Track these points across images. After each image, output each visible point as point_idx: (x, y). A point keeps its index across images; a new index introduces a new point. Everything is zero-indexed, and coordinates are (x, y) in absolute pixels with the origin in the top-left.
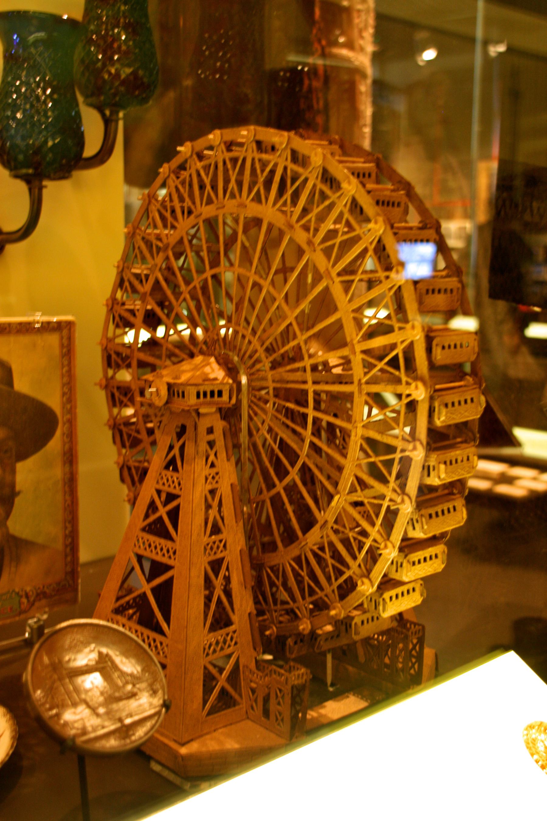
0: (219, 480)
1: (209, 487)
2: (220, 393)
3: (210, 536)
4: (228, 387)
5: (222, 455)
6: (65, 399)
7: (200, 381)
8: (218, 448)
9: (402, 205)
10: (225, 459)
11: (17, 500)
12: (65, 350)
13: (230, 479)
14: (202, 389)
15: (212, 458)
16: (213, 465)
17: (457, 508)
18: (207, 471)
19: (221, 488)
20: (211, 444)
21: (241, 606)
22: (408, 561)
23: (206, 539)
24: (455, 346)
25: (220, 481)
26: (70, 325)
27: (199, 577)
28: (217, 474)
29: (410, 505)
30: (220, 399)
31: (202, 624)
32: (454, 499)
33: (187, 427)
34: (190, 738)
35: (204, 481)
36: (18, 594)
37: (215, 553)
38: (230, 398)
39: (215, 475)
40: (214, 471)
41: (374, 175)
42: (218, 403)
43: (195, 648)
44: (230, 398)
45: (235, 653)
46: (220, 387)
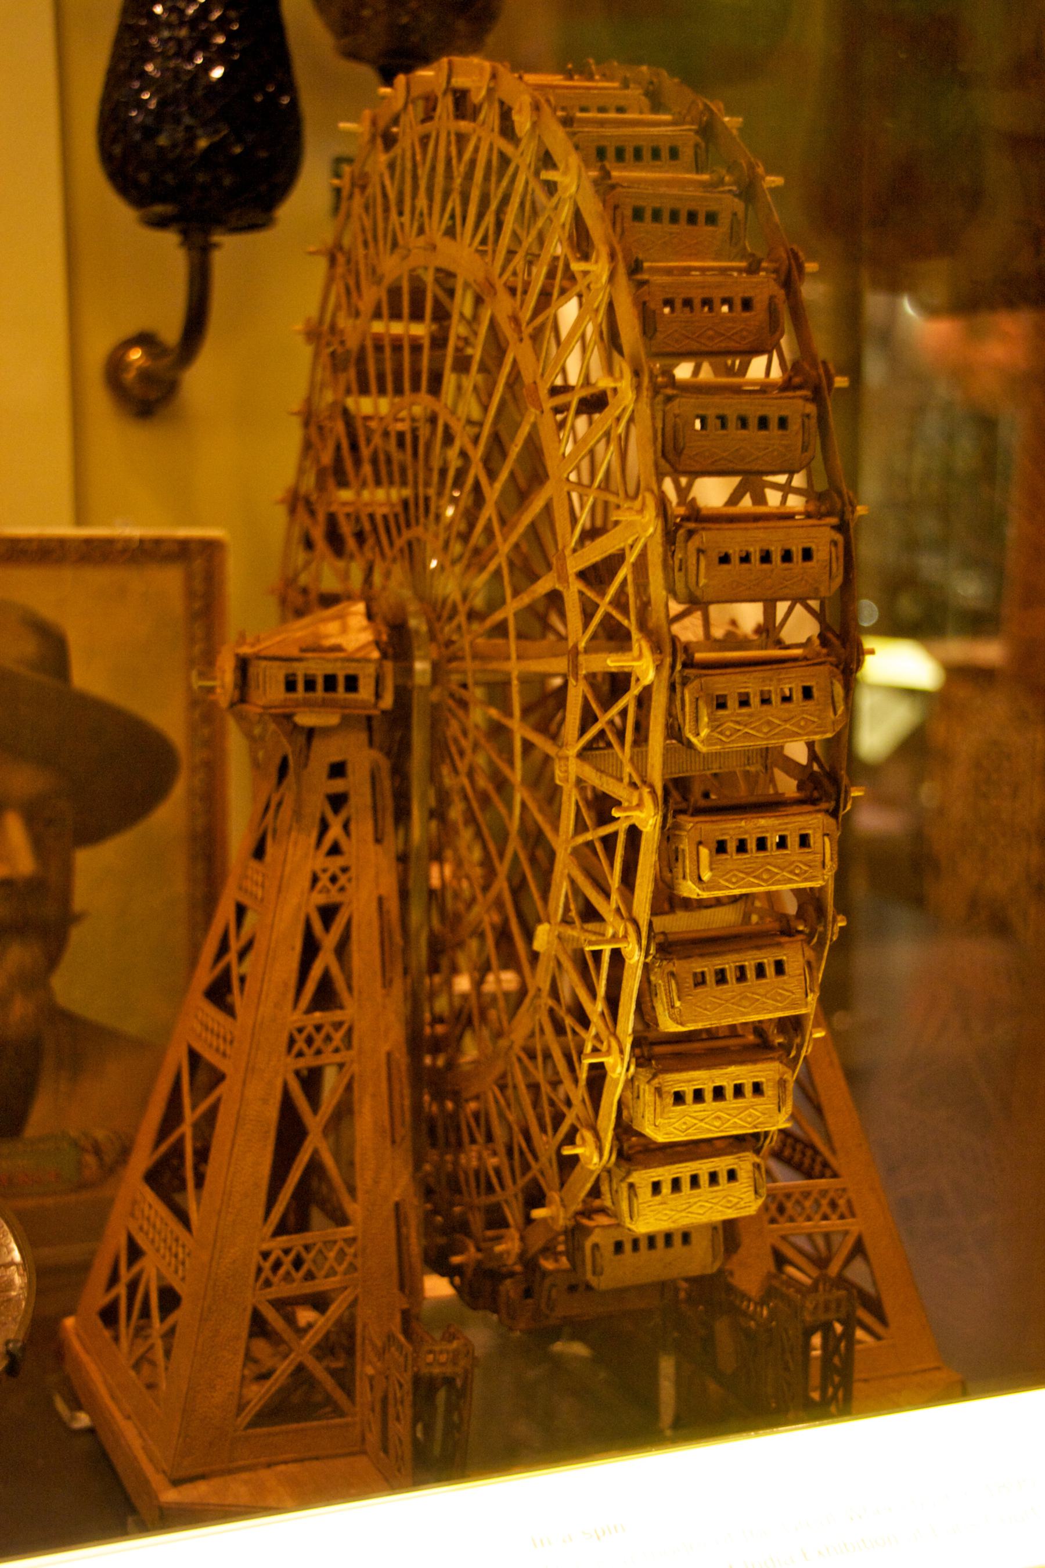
0: (347, 885)
1: (319, 898)
2: (352, 683)
3: (309, 1011)
4: (371, 669)
5: (363, 828)
6: (197, 714)
7: (295, 652)
8: (353, 810)
9: (724, 220)
10: (370, 838)
11: (77, 935)
12: (197, 605)
13: (377, 885)
14: (300, 670)
15: (335, 832)
16: (335, 850)
17: (787, 968)
18: (319, 861)
19: (350, 903)
20: (338, 801)
21: (376, 1182)
22: (659, 1091)
23: (296, 1018)
24: (787, 556)
25: (351, 888)
26: (211, 548)
27: (265, 1101)
28: (345, 870)
29: (637, 947)
30: (351, 696)
31: (261, 1211)
32: (779, 945)
33: (637, 824)
34: (199, 1470)
35: (307, 884)
36: (75, 1144)
37: (319, 1052)
38: (378, 695)
39: (339, 873)
40: (338, 861)
41: (687, 153)
42: (344, 705)
43: (234, 1262)
44: (378, 695)
45: (346, 1293)
46: (352, 669)
